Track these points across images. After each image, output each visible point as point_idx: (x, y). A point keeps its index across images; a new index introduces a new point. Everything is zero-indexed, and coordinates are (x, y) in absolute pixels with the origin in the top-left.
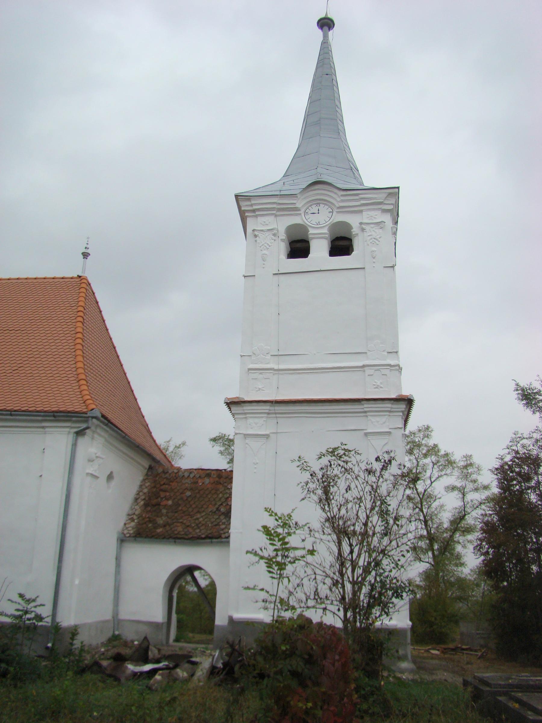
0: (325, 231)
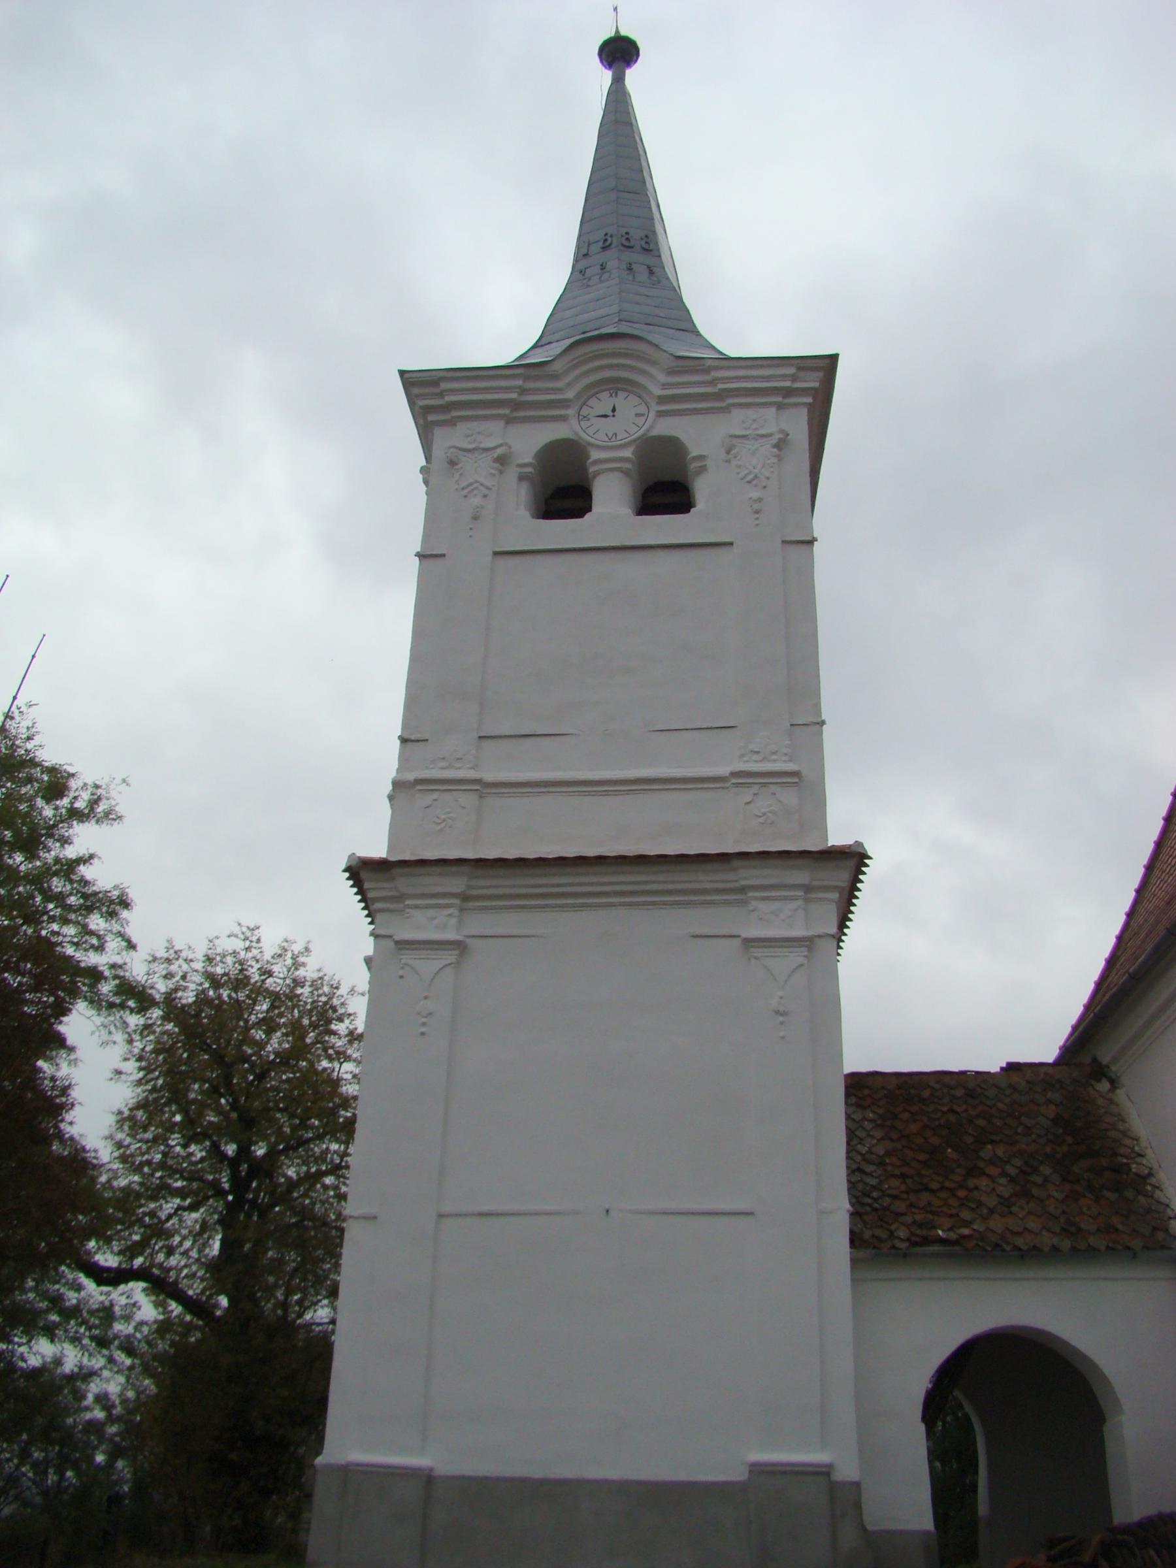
0: (628, 453)
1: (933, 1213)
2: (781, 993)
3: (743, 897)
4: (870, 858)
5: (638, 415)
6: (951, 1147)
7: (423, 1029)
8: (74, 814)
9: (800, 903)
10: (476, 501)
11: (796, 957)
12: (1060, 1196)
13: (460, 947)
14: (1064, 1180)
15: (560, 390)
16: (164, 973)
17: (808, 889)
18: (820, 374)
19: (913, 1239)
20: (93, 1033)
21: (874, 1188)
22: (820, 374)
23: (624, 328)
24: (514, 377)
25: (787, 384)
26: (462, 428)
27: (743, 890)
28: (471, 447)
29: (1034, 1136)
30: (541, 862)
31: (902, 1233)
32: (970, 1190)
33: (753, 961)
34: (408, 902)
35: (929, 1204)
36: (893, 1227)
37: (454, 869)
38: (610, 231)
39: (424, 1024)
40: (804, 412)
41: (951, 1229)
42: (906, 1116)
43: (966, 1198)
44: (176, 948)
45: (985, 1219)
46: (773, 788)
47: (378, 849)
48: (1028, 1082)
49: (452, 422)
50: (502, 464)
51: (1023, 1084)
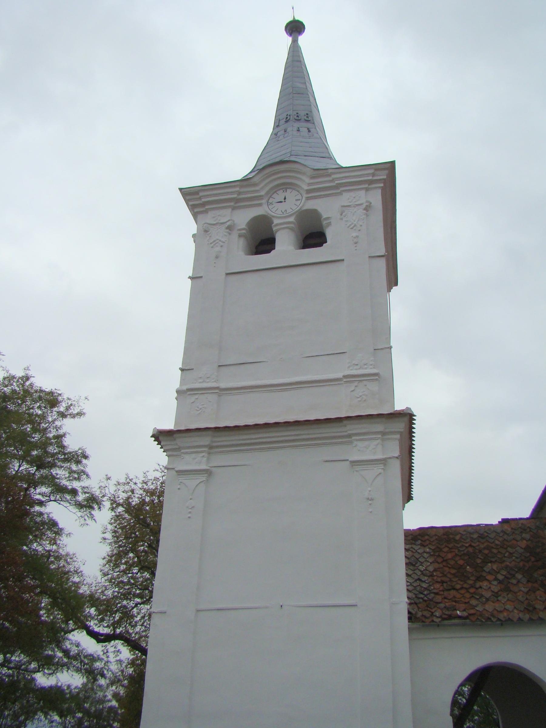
0: (292, 219)
1: (455, 602)
2: (369, 489)
3: (350, 439)
4: (415, 416)
5: (297, 200)
6: (469, 565)
7: (189, 515)
8: (63, 415)
9: (379, 441)
10: (218, 249)
11: (378, 469)
12: (526, 590)
13: (208, 473)
14: (528, 581)
15: (257, 191)
16: (123, 490)
17: (383, 434)
18: (386, 172)
19: (444, 616)
20: (76, 520)
21: (426, 589)
22: (386, 172)
23: (292, 159)
24: (235, 186)
25: (370, 178)
26: (211, 214)
27: (350, 436)
28: (215, 223)
29: (514, 558)
30: (247, 427)
31: (437, 614)
32: (477, 589)
33: (355, 472)
34: (183, 451)
35: (454, 597)
36: (433, 611)
37: (204, 433)
38: (289, 113)
39: (190, 512)
40: (379, 191)
41: (464, 610)
42: (446, 549)
43: (474, 593)
44: (130, 478)
45: (484, 604)
46: (365, 383)
47: (169, 425)
48: (512, 529)
49: (206, 212)
50: (230, 230)
51: (509, 529)
